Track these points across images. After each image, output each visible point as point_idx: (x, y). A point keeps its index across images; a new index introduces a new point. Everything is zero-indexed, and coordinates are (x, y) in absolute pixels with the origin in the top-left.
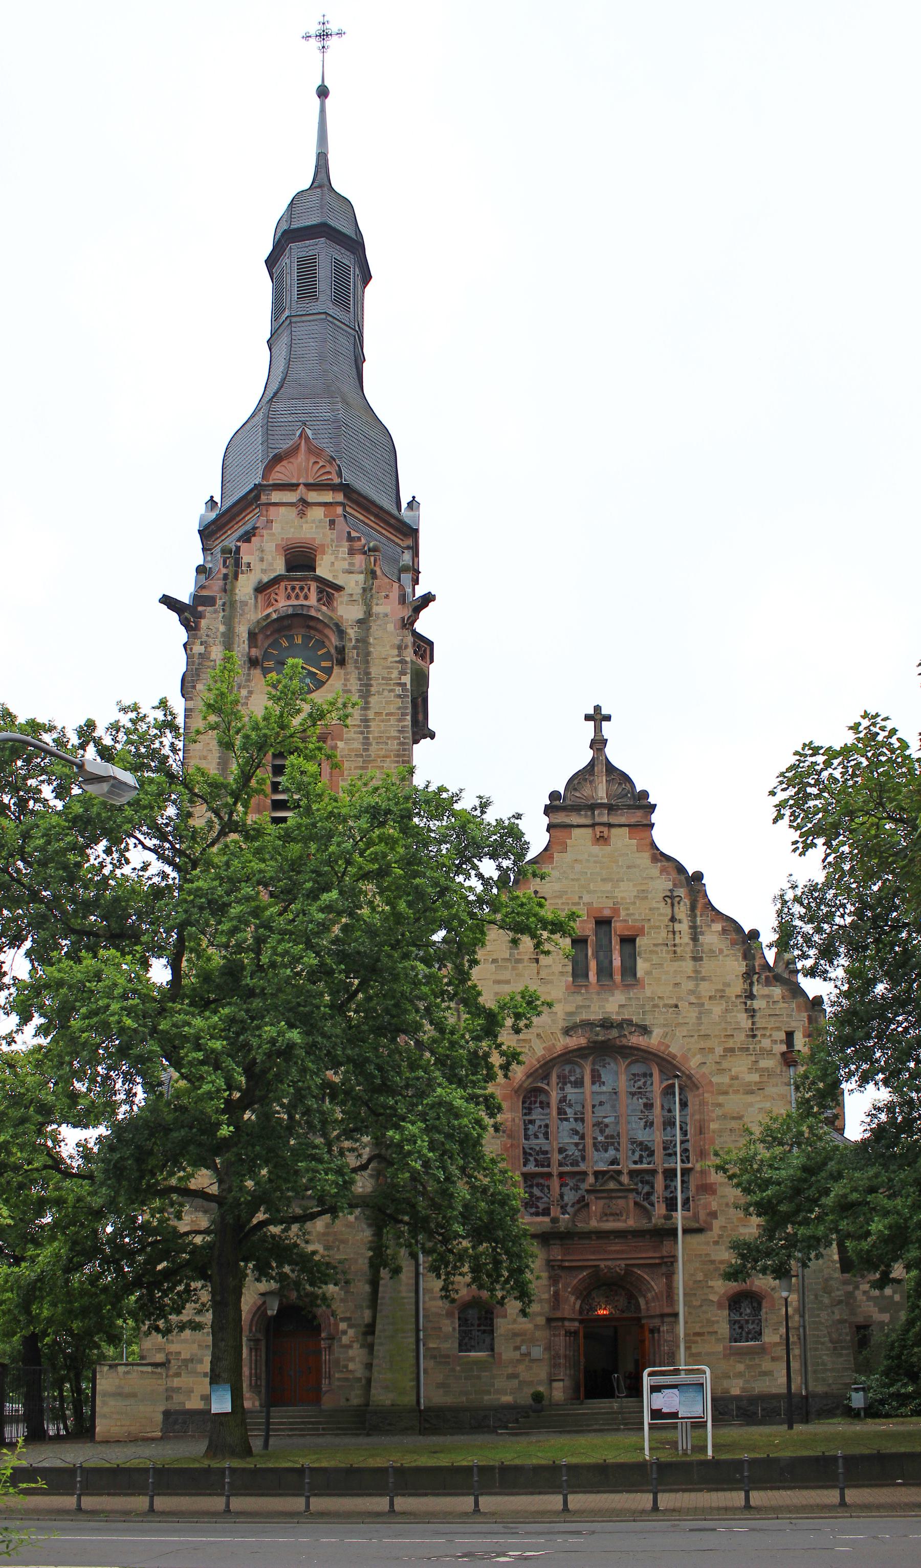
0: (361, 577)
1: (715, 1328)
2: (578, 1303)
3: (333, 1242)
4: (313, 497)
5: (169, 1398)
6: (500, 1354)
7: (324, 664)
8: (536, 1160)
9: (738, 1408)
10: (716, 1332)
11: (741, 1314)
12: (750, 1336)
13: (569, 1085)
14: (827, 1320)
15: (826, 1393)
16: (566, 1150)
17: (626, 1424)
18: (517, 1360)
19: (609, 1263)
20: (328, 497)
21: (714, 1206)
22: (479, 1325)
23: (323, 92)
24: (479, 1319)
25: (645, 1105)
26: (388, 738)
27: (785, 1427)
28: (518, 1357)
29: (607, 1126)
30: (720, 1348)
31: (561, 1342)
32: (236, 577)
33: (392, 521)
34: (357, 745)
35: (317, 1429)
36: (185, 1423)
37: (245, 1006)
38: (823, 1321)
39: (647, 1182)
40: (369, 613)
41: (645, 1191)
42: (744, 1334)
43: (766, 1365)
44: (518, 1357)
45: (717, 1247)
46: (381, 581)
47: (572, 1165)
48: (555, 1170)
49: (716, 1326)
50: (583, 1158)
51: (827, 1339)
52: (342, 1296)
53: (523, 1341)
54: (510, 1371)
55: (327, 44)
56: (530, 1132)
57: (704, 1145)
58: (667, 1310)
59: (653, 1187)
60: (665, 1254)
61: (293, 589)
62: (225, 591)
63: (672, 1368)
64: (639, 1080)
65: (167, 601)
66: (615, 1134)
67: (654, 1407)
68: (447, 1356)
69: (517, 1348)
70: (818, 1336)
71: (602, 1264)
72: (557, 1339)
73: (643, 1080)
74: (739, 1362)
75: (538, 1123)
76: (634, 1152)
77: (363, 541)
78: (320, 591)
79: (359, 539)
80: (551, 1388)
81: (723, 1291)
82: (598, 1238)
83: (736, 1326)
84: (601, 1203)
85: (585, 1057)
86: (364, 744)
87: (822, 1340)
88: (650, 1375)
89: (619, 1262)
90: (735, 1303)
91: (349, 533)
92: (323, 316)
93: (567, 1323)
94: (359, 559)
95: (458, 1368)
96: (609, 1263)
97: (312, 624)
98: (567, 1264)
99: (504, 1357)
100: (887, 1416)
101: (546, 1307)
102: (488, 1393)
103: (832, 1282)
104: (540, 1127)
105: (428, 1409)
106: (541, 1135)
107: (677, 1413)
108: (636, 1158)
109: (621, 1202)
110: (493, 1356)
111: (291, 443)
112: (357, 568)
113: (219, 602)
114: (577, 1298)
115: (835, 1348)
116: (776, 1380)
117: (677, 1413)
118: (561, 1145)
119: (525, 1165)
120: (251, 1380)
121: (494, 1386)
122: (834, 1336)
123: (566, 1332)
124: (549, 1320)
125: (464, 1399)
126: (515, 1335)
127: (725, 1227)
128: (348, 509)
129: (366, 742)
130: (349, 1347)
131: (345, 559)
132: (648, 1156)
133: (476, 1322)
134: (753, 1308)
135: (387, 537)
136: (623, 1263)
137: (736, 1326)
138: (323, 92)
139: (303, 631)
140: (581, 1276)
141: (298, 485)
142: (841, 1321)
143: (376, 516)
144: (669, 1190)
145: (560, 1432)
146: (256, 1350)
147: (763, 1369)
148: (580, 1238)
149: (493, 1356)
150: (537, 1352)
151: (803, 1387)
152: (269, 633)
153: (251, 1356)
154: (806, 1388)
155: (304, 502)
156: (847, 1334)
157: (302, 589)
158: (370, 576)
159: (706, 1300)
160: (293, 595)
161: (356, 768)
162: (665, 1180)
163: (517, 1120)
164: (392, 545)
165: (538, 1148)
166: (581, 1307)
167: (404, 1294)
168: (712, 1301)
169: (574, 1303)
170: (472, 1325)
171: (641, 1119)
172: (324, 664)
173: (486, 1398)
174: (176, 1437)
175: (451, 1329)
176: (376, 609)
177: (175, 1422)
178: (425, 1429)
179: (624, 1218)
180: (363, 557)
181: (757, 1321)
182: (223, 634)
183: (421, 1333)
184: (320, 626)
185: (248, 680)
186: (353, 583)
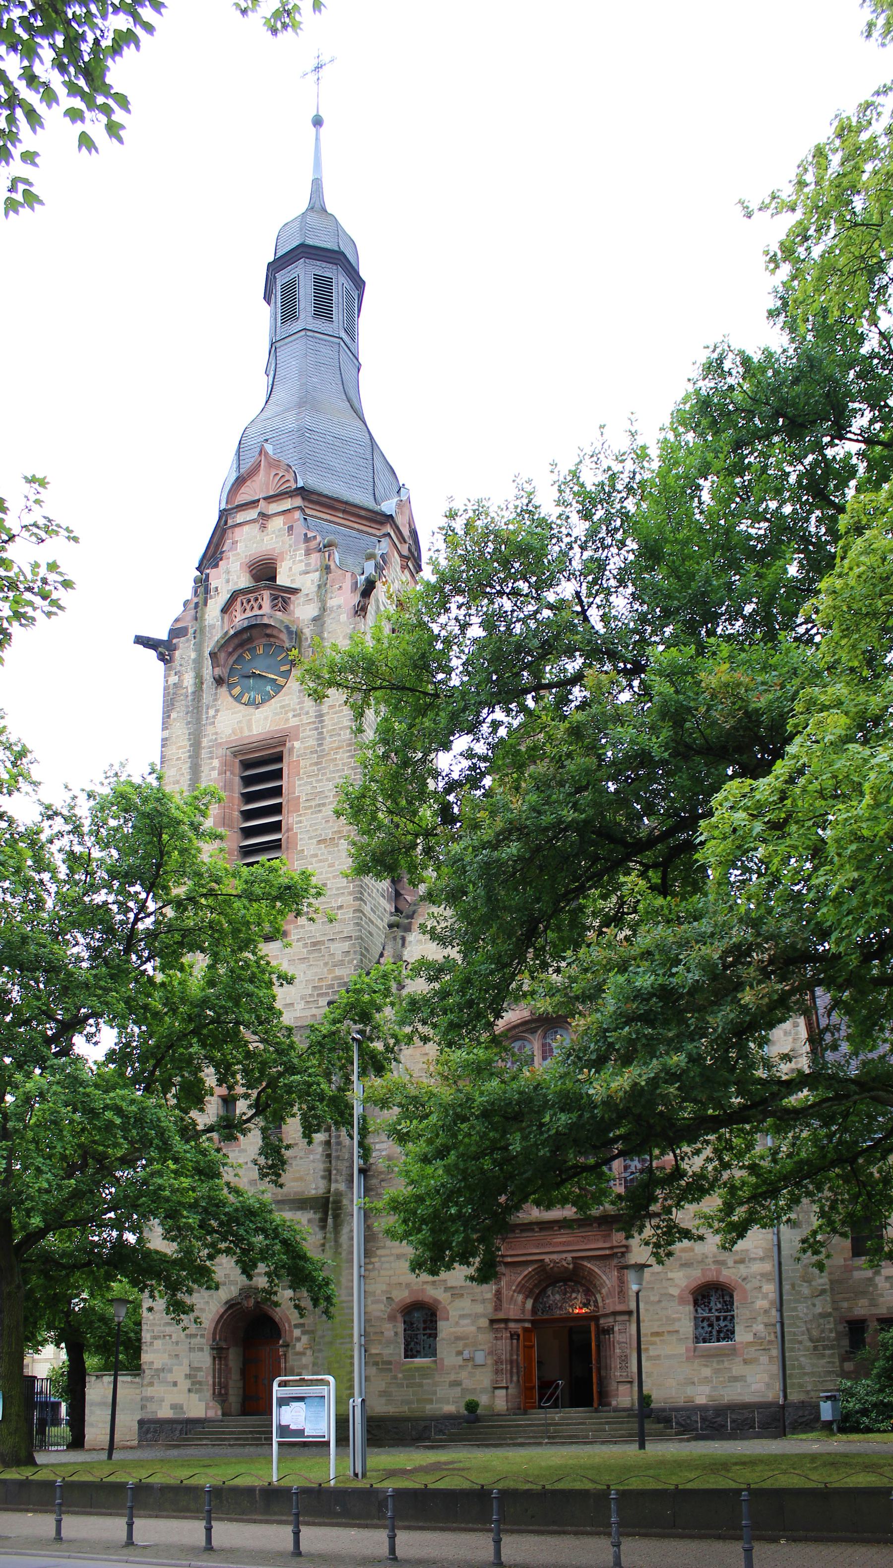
0: (317, 575)
2: (529, 1304)
4: (274, 508)
5: (143, 1407)
6: (442, 1359)
7: (283, 669)
9: (703, 1419)
10: (677, 1332)
11: (710, 1310)
12: (722, 1335)
14: (806, 1314)
15: (803, 1402)
17: (549, 1437)
18: (460, 1366)
19: (554, 1257)
20: (287, 504)
22: (425, 1329)
23: (318, 122)
24: (425, 1322)
26: (341, 729)
27: (636, 1446)
28: (461, 1363)
30: (681, 1349)
31: (504, 1346)
32: (206, 604)
33: (363, 513)
34: (312, 742)
35: (260, 1439)
36: (155, 1432)
38: (801, 1315)
40: (323, 609)
42: (715, 1333)
43: (738, 1369)
44: (461, 1363)
46: (336, 573)
51: (806, 1337)
53: (465, 1345)
54: (453, 1377)
55: (320, 75)
60: (615, 1244)
61: (249, 601)
62: (196, 619)
63: (298, 1378)
65: (143, 641)
67: (283, 1423)
68: (390, 1363)
69: (460, 1353)
71: (547, 1258)
72: (499, 1342)
74: (706, 1366)
77: (319, 539)
78: (275, 598)
79: (315, 537)
80: (493, 1397)
82: (541, 1229)
83: (705, 1324)
85: (533, 1031)
86: (318, 739)
87: (800, 1338)
88: (280, 1386)
89: (564, 1256)
90: (703, 1297)
91: (306, 535)
92: (303, 333)
93: (512, 1325)
94: (315, 557)
95: (400, 1375)
96: (554, 1257)
97: (269, 631)
98: (509, 1260)
99: (446, 1363)
100: (868, 1430)
102: (431, 1401)
107: (303, 1430)
110: (435, 1362)
111: (252, 460)
112: (312, 567)
113: (191, 631)
114: (527, 1297)
115: (815, 1348)
116: (749, 1386)
117: (303, 1430)
120: (214, 1390)
122: (815, 1333)
123: (512, 1335)
124: (492, 1322)
125: (406, 1408)
126: (458, 1338)
128: (308, 511)
129: (321, 738)
130: (303, 1354)
131: (301, 561)
133: (422, 1326)
135: (358, 530)
136: (569, 1256)
137: (705, 1324)
138: (318, 122)
139: (264, 641)
140: (526, 1272)
141: (258, 501)
142: (823, 1315)
143: (344, 512)
145: (478, 1446)
146: (220, 1358)
148: (522, 1231)
150: (480, 1357)
151: (781, 1394)
152: (230, 650)
153: (214, 1364)
154: (785, 1397)
155: (263, 516)
156: (831, 1331)
157: (256, 599)
158: (324, 572)
159: (665, 1294)
160: (248, 608)
161: (311, 765)
164: (365, 537)
166: (534, 1307)
168: (673, 1296)
169: (524, 1303)
172: (283, 669)
173: (428, 1407)
174: (148, 1446)
175: (392, 1334)
176: (331, 603)
177: (148, 1432)
180: (318, 554)
182: (194, 661)
184: (275, 633)
185: (215, 700)
186: (308, 583)
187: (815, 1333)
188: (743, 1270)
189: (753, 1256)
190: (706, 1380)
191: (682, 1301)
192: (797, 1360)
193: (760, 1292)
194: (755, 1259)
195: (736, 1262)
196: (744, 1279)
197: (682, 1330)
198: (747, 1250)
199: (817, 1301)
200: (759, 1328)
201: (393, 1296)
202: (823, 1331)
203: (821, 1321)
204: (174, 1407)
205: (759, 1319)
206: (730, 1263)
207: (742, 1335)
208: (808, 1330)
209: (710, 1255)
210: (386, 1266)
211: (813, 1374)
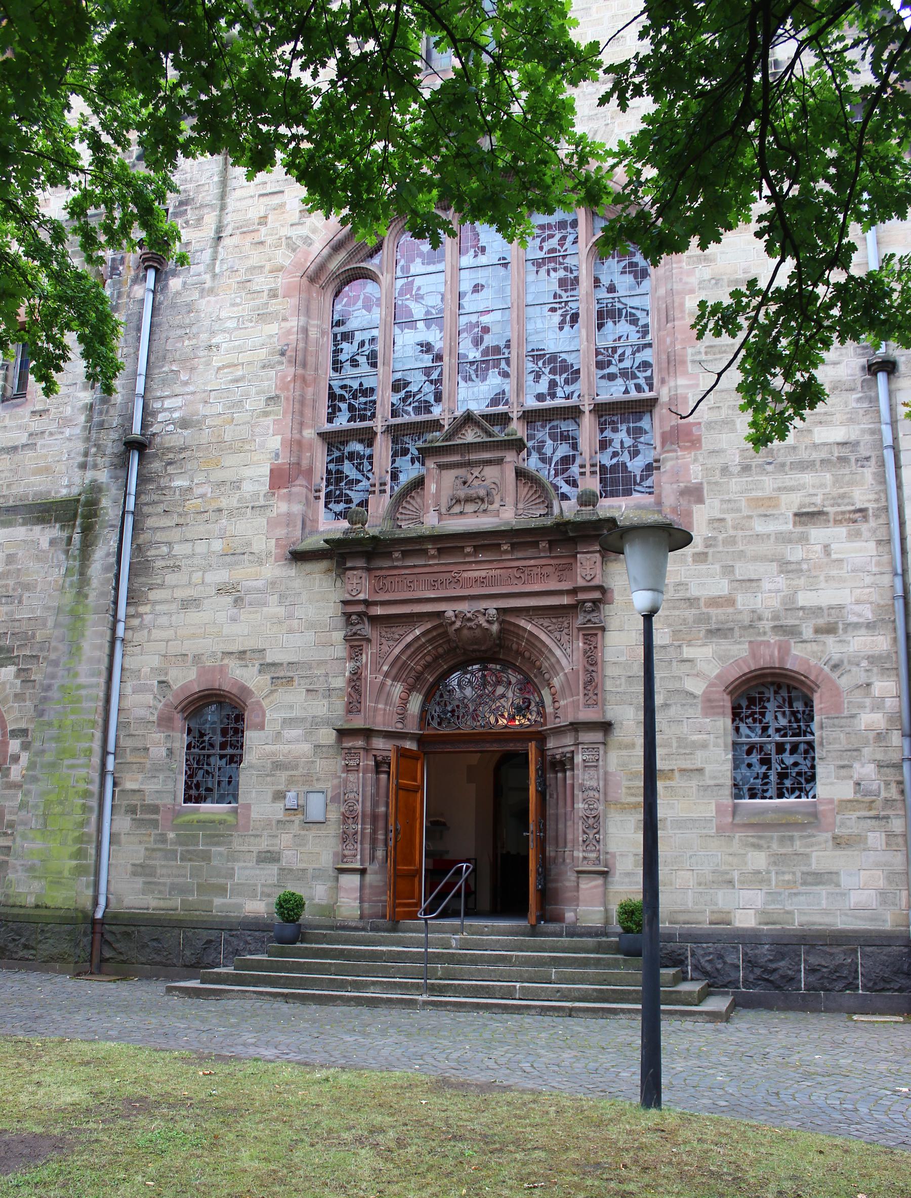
1: (699, 759)
2: (415, 704)
3: (14, 590)
6: (248, 807)
8: (351, 408)
9: (750, 963)
10: (700, 770)
11: (765, 729)
12: (788, 783)
13: (418, 260)
16: (407, 384)
18: (279, 822)
19: (464, 607)
21: (696, 474)
22: (223, 746)
25: (562, 282)
28: (281, 816)
29: (486, 330)
39: (565, 437)
41: (559, 454)
42: (773, 778)
44: (281, 816)
45: (703, 567)
47: (418, 410)
48: (378, 424)
49: (700, 754)
50: (438, 398)
52: (18, 691)
53: (291, 781)
54: (264, 844)
56: (343, 357)
57: (673, 343)
58: (587, 715)
59: (575, 447)
60: (581, 582)
64: (552, 236)
66: (502, 344)
68: (155, 809)
69: (279, 796)
71: (449, 609)
73: (558, 236)
75: (359, 337)
76: (538, 376)
80: (336, 889)
81: (716, 672)
83: (755, 758)
84: (449, 476)
89: (482, 605)
90: (752, 701)
95: (171, 835)
96: (464, 607)
98: (379, 611)
99: (254, 815)
101: (339, 705)
102: (221, 890)
104: (362, 344)
105: (112, 918)
106: (362, 360)
108: (543, 387)
109: (490, 472)
114: (410, 689)
118: (398, 375)
119: (330, 420)
121: (232, 876)
124: (343, 733)
126: (278, 766)
127: (722, 520)
132: (567, 382)
133: (218, 739)
134: (794, 713)
136: (492, 606)
137: (755, 758)
140: (409, 638)
144: (610, 450)
147: (814, 867)
148: (405, 554)
149: (235, 811)
150: (316, 806)
159: (677, 691)
162: (602, 431)
163: (313, 333)
165: (355, 385)
166: (424, 711)
167: (82, 680)
169: (405, 702)
170: (212, 746)
171: (553, 310)
173: (218, 901)
178: (104, 960)
179: (496, 506)
181: (802, 747)
183: (111, 758)
188: (832, 647)
189: (853, 619)
191: (710, 706)
193: (868, 695)
194: (856, 626)
195: (817, 631)
196: (835, 667)
197: (708, 769)
198: (841, 607)
200: (866, 770)
201: (169, 678)
205: (866, 751)
206: (808, 632)
209: (767, 614)
210: (163, 620)
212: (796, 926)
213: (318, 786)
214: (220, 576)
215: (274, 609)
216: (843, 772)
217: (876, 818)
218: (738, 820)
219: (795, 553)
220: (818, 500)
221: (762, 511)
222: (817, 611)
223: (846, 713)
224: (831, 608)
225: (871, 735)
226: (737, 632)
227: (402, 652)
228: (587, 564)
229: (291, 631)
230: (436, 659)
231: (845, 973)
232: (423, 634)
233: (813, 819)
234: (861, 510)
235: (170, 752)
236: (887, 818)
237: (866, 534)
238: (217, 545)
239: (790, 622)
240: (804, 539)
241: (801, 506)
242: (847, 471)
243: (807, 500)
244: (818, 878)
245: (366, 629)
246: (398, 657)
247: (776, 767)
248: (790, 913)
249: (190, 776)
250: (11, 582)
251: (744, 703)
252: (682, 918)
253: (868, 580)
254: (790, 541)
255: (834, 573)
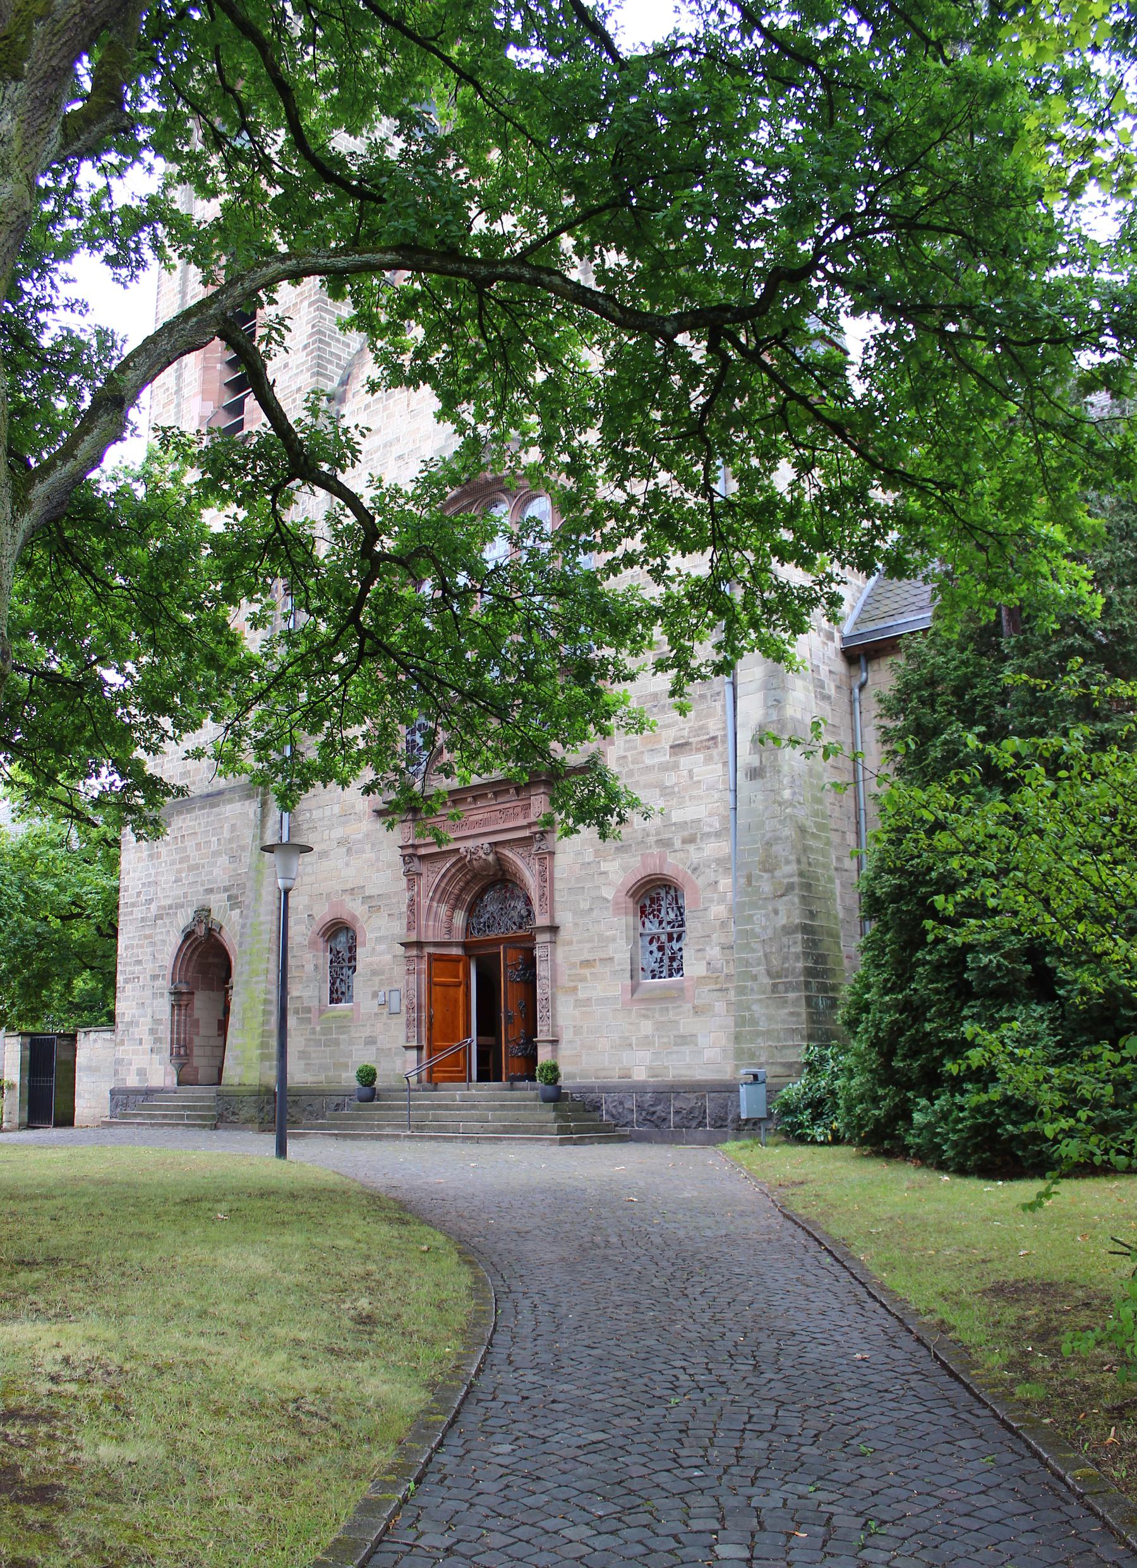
2: (459, 919)
6: (358, 1004)
10: (611, 959)
14: (765, 928)
19: (470, 844)
28: (376, 1010)
37: (596, 337)
43: (687, 1023)
44: (376, 1010)
51: (762, 969)
53: (381, 983)
54: (367, 1032)
70: (748, 964)
74: (646, 1017)
87: (755, 970)
98: (423, 851)
103: (777, 849)
114: (454, 908)
121: (351, 1056)
122: (775, 962)
126: (374, 973)
147: (682, 1031)
168: (606, 899)
187: (775, 962)
188: (694, 855)
189: (707, 829)
190: (646, 1042)
191: (617, 911)
192: (749, 1009)
193: (716, 890)
194: (709, 835)
195: (684, 842)
196: (695, 869)
197: (617, 956)
198: (699, 821)
199: (781, 905)
200: (714, 952)
201: (313, 913)
202: (786, 959)
203: (785, 940)
204: (141, 1073)
205: (714, 936)
206: (678, 844)
207: (693, 967)
208: (766, 955)
210: (309, 869)
211: (768, 1034)
212: (670, 1078)
213: (396, 986)
214: (338, 833)
215: (369, 855)
216: (700, 955)
217: (720, 990)
218: (636, 996)
219: (670, 779)
220: (686, 733)
221: (649, 747)
222: (684, 825)
223: (702, 907)
224: (693, 822)
225: (718, 923)
226: (634, 848)
227: (441, 880)
228: (537, 804)
229: (378, 871)
230: (467, 883)
231: (696, 1113)
232: (453, 865)
233: (679, 995)
234: (713, 738)
235: (316, 966)
236: (727, 989)
237: (716, 757)
238: (336, 809)
239: (667, 836)
240: (676, 766)
241: (675, 739)
242: (704, 706)
243: (679, 734)
244: (684, 1040)
245: (416, 866)
246: (438, 885)
247: (668, 952)
248: (667, 1068)
249: (333, 984)
250: (234, 846)
251: (648, 903)
252: (602, 1074)
253: (717, 796)
254: (667, 770)
255: (695, 793)
